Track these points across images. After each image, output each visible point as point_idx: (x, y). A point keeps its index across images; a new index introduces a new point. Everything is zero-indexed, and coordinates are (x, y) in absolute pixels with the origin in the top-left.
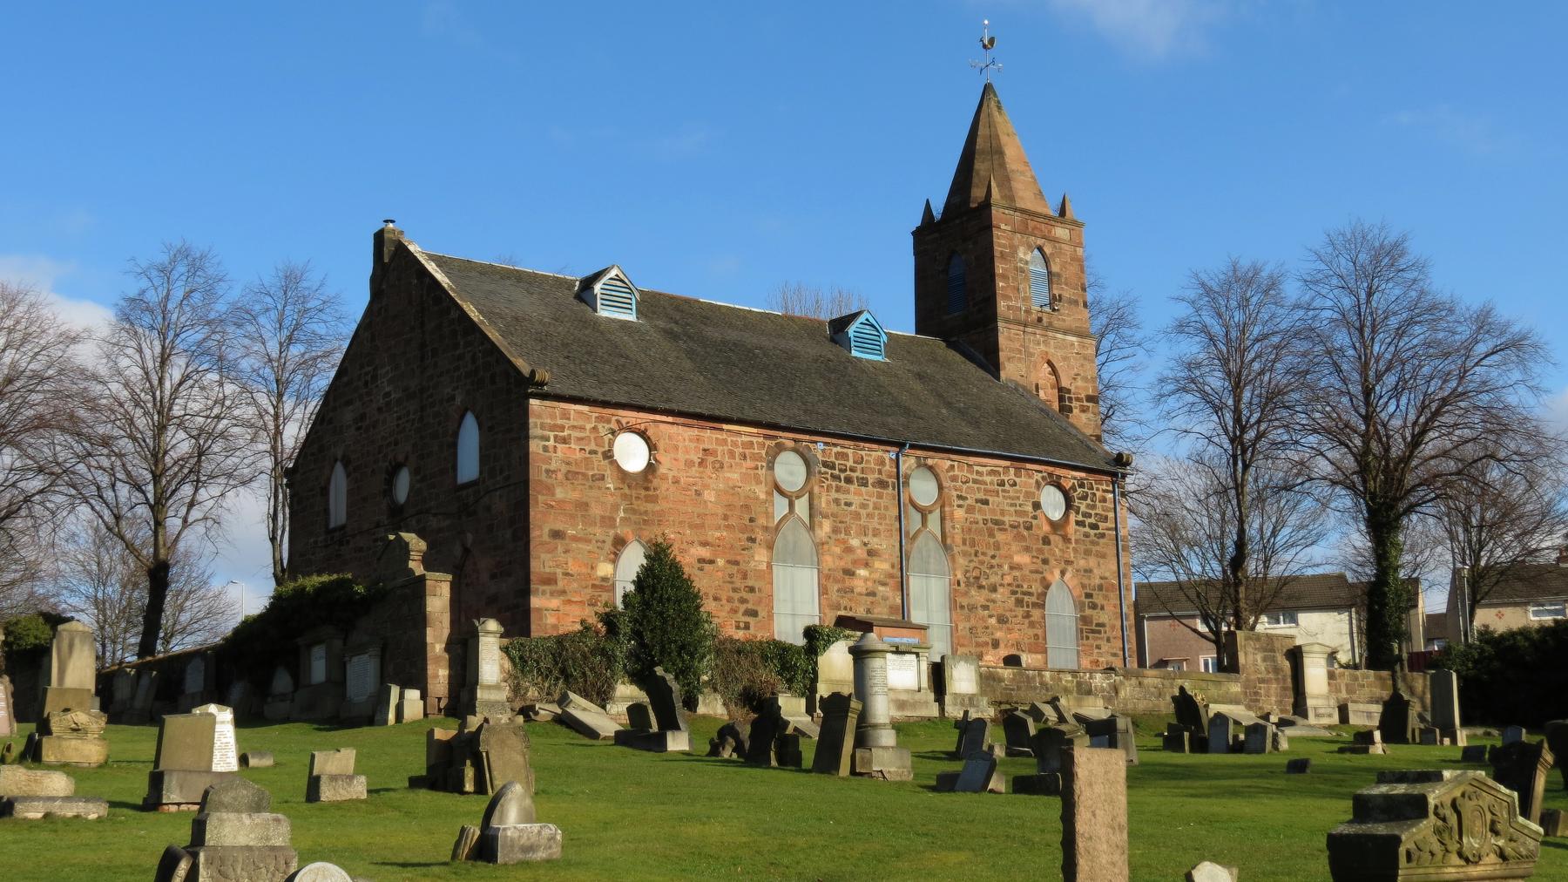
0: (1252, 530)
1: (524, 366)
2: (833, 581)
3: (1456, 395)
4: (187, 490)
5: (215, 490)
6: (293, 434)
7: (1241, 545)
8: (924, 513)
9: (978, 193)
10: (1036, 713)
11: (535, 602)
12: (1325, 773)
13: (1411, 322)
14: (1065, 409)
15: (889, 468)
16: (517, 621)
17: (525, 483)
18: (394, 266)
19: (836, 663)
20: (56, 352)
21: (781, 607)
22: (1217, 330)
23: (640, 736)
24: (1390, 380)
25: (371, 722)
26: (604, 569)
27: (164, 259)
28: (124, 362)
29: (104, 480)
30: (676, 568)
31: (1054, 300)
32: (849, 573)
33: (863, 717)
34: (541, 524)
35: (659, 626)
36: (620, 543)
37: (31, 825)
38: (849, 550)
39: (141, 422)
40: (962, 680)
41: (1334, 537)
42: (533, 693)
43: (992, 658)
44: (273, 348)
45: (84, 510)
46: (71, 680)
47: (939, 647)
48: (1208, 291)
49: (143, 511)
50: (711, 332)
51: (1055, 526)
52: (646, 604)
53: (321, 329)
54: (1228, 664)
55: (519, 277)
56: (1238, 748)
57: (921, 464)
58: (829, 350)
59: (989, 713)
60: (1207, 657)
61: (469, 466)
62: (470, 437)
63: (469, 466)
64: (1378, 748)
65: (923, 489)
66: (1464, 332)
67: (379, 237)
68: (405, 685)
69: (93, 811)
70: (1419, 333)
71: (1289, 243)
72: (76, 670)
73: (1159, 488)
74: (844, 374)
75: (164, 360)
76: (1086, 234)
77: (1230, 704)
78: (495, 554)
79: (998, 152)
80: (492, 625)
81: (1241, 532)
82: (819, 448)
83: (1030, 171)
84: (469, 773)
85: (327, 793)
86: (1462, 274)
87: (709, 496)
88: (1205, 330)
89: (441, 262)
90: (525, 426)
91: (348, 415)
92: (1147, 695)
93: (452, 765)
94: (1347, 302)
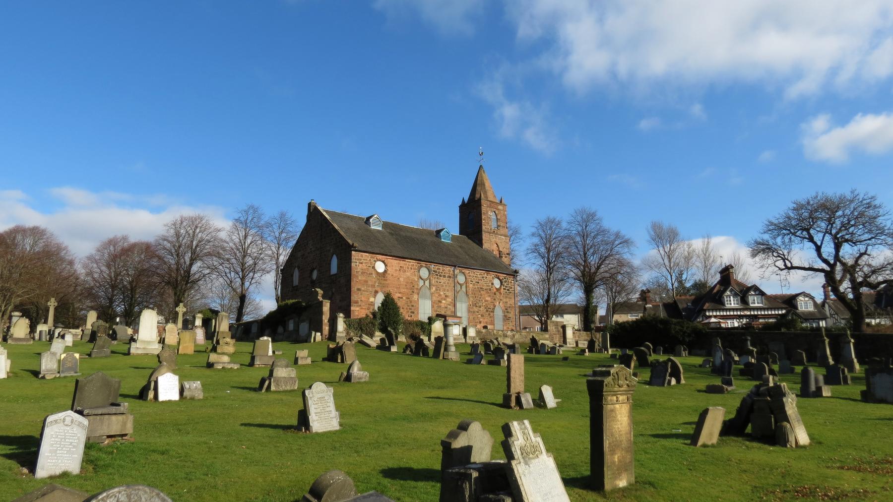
0: (552, 292)
1: (350, 242)
2: (436, 304)
3: (610, 255)
4: (251, 274)
5: (259, 274)
6: (283, 259)
7: (549, 296)
8: (461, 285)
9: (477, 196)
10: (492, 342)
11: (352, 308)
12: (572, 360)
13: (597, 234)
14: (501, 257)
15: (452, 272)
16: (348, 314)
17: (350, 275)
18: (313, 213)
19: (437, 327)
20: (214, 234)
21: (421, 311)
22: (543, 235)
23: (383, 347)
24: (592, 251)
25: (306, 341)
26: (372, 299)
27: (246, 208)
28: (234, 237)
29: (227, 271)
30: (393, 300)
31: (498, 226)
32: (440, 302)
33: (446, 343)
34: (354, 286)
35: (388, 316)
36: (376, 292)
37: (219, 370)
38: (440, 295)
39: (238, 255)
40: (471, 332)
41: (575, 294)
42: (352, 334)
43: (479, 326)
44: (277, 234)
45: (221, 280)
46: (222, 329)
47: (465, 323)
48: (541, 225)
49: (239, 280)
50: (402, 233)
51: (497, 290)
52: (384, 310)
53: (291, 229)
54: (545, 329)
55: (349, 217)
56: (548, 353)
57: (461, 272)
58: (435, 239)
59: (479, 342)
60: (538, 327)
61: (334, 270)
62: (334, 262)
63: (334, 270)
64: (587, 354)
65: (461, 279)
66: (612, 238)
67: (309, 204)
68: (316, 331)
69: (236, 367)
70: (600, 238)
71: (564, 213)
72: (223, 325)
73: (526, 279)
74: (439, 246)
75: (246, 237)
76: (507, 208)
77: (545, 341)
78: (341, 293)
79: (483, 184)
80: (341, 315)
81: (549, 292)
82: (432, 266)
83: (492, 190)
84: (339, 357)
85: (300, 362)
86: (612, 221)
87: (401, 279)
88: (540, 235)
89: (327, 212)
90: (350, 259)
91: (299, 254)
92: (523, 338)
93: (334, 355)
94: (580, 229)
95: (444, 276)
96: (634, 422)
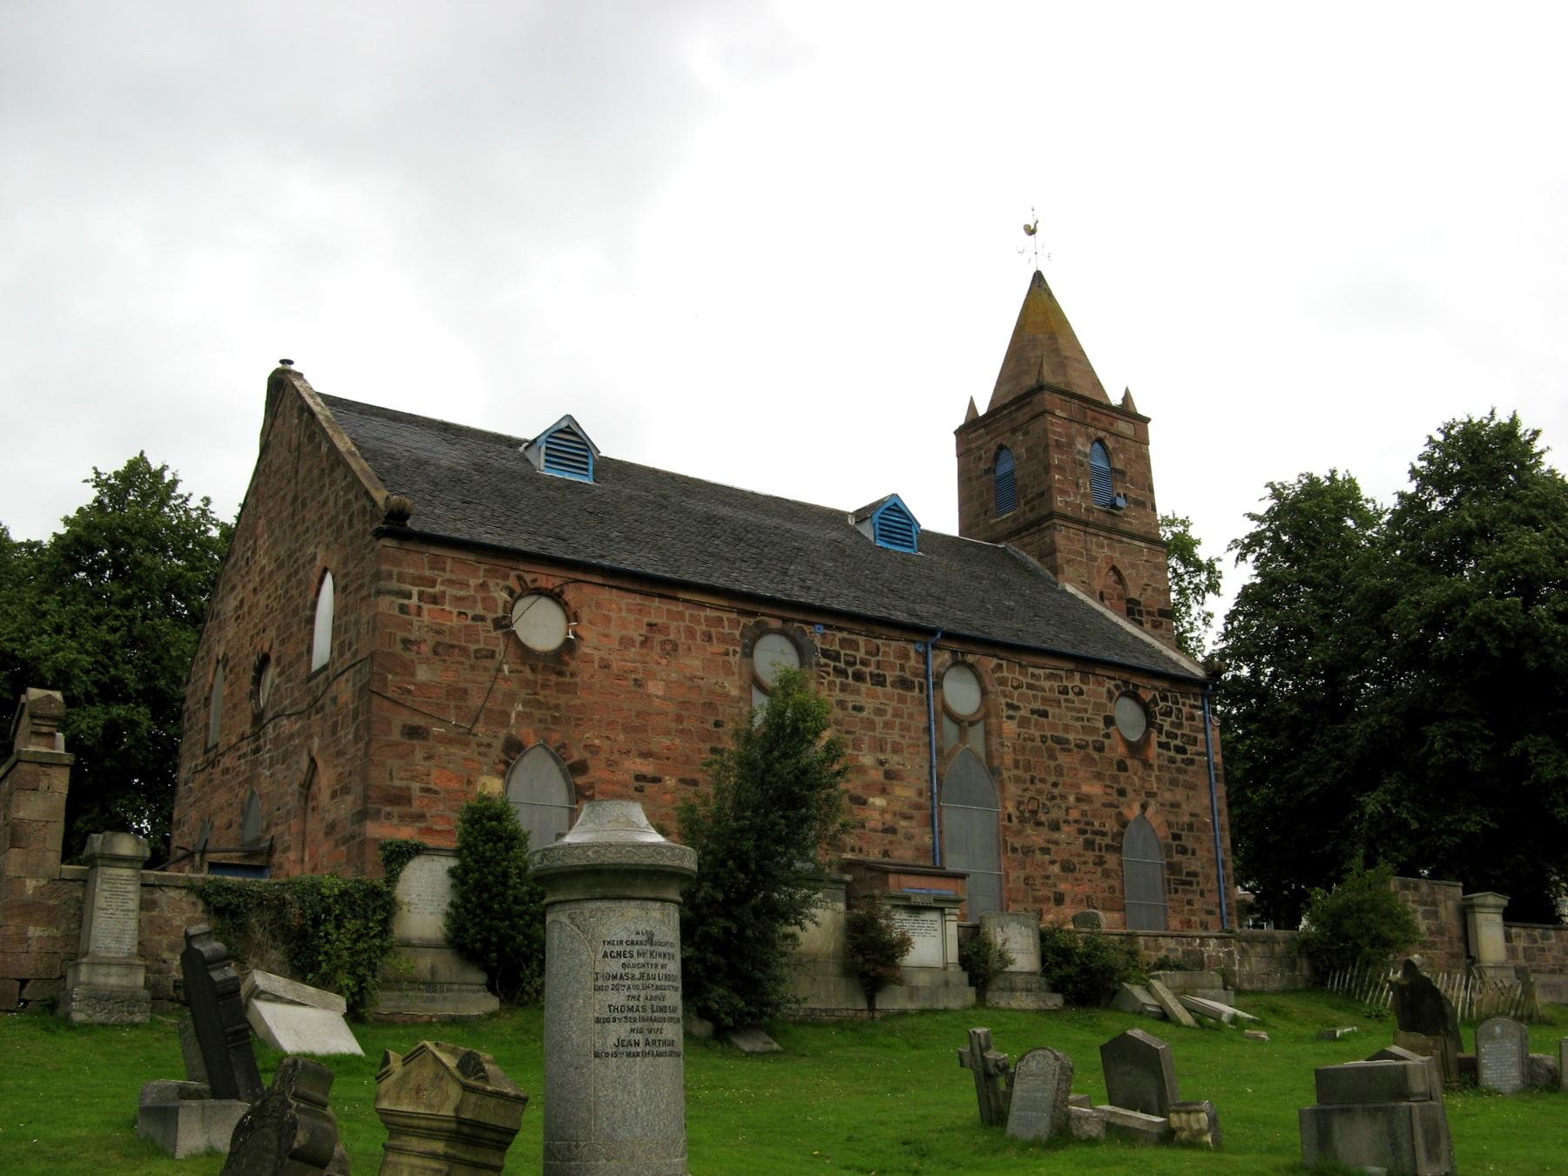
50: (690, 504)
51: (1136, 749)
82: (816, 636)
87: (655, 688)
95: (879, 681)
96: (1136, 1000)
